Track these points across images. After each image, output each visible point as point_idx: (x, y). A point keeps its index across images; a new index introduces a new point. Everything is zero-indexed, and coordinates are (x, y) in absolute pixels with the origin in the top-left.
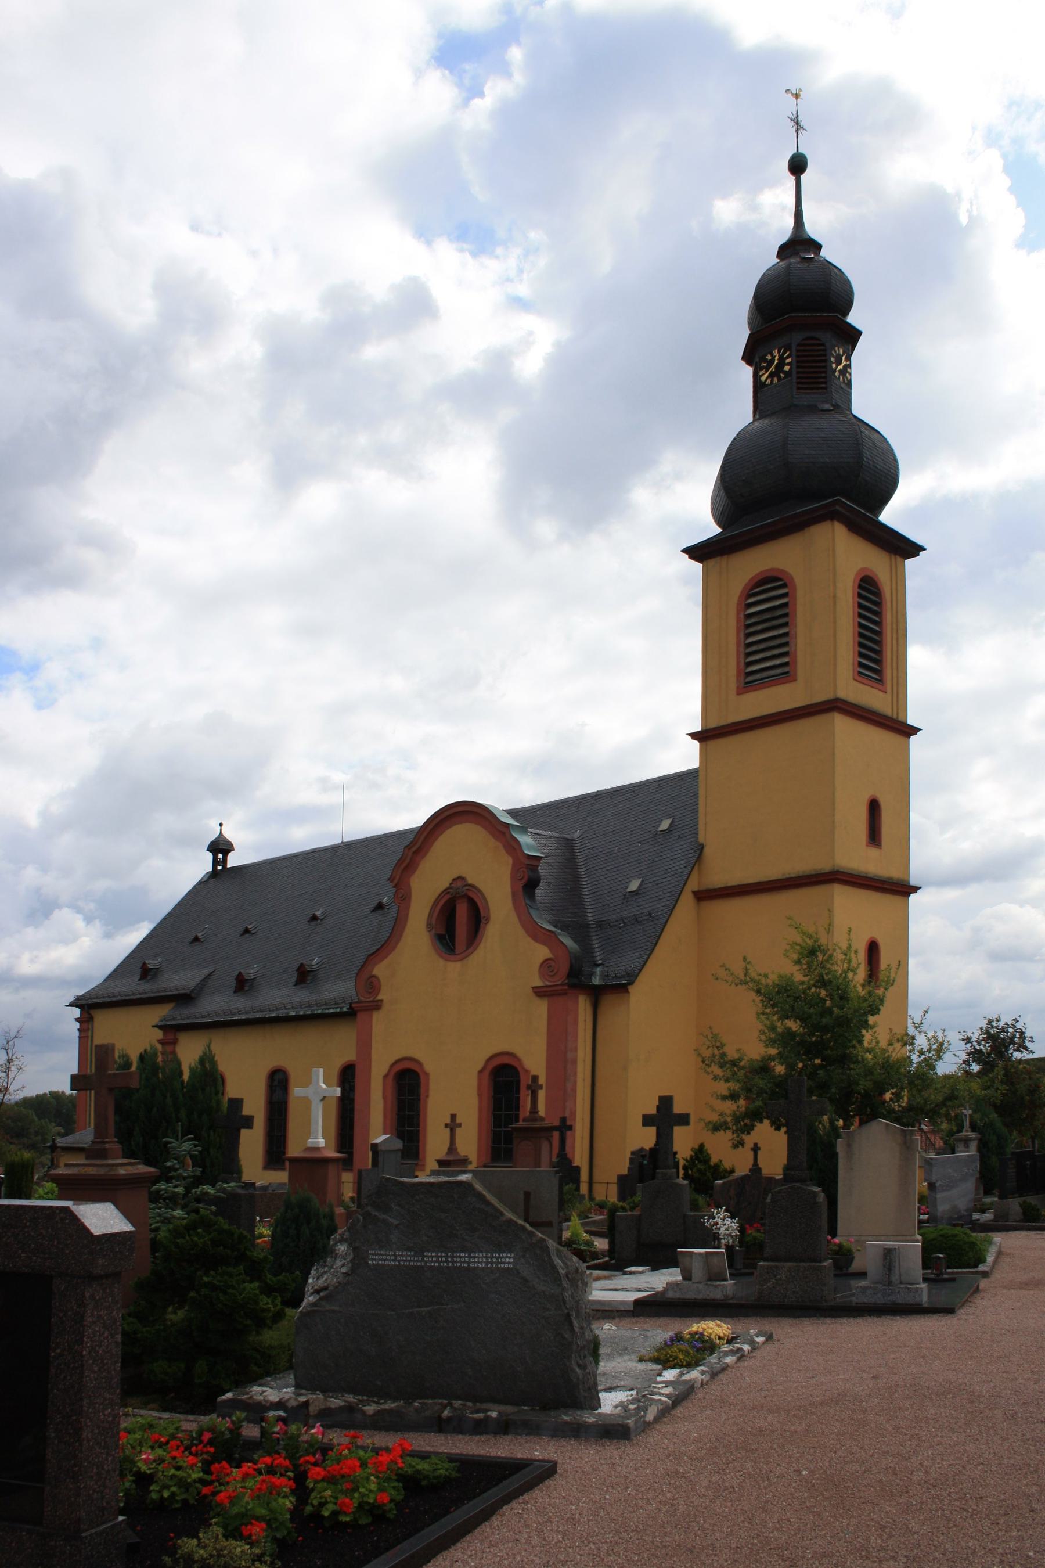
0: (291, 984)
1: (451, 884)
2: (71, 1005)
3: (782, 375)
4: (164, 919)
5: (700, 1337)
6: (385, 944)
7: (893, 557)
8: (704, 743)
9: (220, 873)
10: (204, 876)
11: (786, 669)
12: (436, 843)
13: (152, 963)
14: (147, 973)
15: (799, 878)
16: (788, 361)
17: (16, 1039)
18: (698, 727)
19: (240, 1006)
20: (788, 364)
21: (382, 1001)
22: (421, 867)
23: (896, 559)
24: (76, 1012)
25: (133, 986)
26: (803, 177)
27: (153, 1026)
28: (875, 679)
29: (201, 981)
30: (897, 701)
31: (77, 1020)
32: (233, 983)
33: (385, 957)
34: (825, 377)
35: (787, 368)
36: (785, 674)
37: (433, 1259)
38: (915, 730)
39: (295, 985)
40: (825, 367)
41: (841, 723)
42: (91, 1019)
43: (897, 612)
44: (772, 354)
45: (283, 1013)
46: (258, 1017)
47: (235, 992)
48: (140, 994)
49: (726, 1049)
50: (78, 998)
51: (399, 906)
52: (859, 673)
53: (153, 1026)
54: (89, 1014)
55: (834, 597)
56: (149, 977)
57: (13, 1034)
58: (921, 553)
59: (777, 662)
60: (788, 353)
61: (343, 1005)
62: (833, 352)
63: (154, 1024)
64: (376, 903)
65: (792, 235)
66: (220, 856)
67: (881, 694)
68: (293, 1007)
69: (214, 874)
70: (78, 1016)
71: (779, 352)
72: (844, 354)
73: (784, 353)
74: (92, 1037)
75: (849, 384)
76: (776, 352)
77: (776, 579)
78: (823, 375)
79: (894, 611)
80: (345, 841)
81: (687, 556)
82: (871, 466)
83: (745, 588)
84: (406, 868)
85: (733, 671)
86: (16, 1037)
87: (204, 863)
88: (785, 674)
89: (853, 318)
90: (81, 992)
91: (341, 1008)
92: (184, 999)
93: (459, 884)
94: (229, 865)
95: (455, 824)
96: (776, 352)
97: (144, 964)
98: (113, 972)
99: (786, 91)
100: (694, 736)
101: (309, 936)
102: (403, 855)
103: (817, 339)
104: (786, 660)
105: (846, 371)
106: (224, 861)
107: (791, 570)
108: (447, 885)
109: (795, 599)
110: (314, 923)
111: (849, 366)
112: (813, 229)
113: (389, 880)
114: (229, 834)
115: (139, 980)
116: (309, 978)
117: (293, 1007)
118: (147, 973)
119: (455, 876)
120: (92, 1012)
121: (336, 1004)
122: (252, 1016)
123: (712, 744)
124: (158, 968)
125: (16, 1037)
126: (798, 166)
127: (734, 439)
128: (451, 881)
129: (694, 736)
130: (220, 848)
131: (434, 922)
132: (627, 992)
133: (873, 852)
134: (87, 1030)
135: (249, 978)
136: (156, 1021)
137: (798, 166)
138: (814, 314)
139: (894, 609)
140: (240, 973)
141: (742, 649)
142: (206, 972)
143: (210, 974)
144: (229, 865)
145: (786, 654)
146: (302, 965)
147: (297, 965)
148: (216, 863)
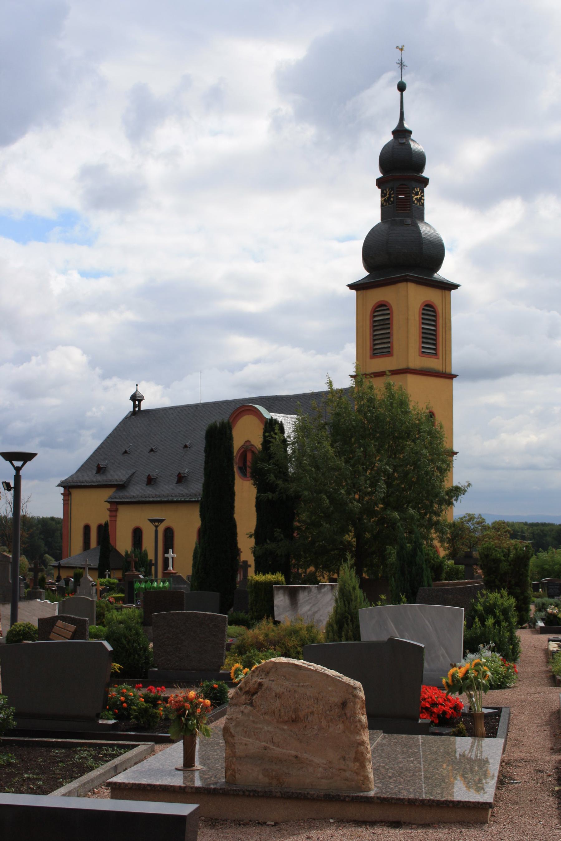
1: (244, 443)
2: (59, 485)
3: (390, 202)
4: (108, 437)
7: (444, 291)
9: (137, 412)
10: (129, 413)
11: (389, 350)
12: (238, 423)
13: (103, 464)
14: (100, 470)
16: (392, 196)
19: (150, 492)
20: (393, 197)
23: (445, 293)
24: (62, 490)
25: (91, 477)
26: (404, 93)
27: (105, 501)
28: (433, 353)
31: (62, 494)
32: (145, 479)
34: (409, 205)
35: (392, 199)
36: (388, 352)
37: (177, 586)
39: (176, 483)
40: (409, 199)
42: (70, 494)
43: (445, 318)
44: (386, 191)
45: (170, 499)
47: (147, 485)
48: (97, 482)
50: (62, 482)
52: (423, 352)
53: (105, 501)
54: (69, 491)
55: (408, 319)
56: (101, 472)
58: (459, 288)
59: (386, 346)
61: (199, 496)
62: (414, 192)
63: (105, 500)
64: (124, 451)
65: (396, 128)
66: (137, 403)
67: (436, 360)
71: (389, 190)
72: (420, 191)
73: (391, 191)
74: (71, 504)
75: (423, 205)
76: (388, 190)
77: (384, 305)
78: (409, 203)
80: (202, 402)
85: (368, 348)
86: (27, 502)
88: (388, 352)
89: (425, 174)
90: (63, 479)
91: (198, 498)
92: (121, 487)
93: (248, 444)
94: (142, 409)
95: (243, 416)
96: (388, 190)
97: (99, 465)
100: (351, 376)
103: (404, 185)
104: (389, 345)
105: (421, 201)
106: (139, 405)
107: (390, 302)
109: (392, 316)
110: (185, 449)
111: (423, 196)
114: (141, 391)
115: (96, 473)
116: (183, 480)
119: (246, 440)
120: (70, 490)
121: (195, 496)
122: (155, 499)
124: (105, 467)
125: (27, 502)
130: (136, 399)
136: (106, 498)
137: (402, 87)
140: (149, 475)
141: (372, 337)
142: (132, 472)
143: (134, 473)
144: (142, 409)
145: (389, 342)
146: (179, 473)
147: (177, 473)
148: (135, 406)
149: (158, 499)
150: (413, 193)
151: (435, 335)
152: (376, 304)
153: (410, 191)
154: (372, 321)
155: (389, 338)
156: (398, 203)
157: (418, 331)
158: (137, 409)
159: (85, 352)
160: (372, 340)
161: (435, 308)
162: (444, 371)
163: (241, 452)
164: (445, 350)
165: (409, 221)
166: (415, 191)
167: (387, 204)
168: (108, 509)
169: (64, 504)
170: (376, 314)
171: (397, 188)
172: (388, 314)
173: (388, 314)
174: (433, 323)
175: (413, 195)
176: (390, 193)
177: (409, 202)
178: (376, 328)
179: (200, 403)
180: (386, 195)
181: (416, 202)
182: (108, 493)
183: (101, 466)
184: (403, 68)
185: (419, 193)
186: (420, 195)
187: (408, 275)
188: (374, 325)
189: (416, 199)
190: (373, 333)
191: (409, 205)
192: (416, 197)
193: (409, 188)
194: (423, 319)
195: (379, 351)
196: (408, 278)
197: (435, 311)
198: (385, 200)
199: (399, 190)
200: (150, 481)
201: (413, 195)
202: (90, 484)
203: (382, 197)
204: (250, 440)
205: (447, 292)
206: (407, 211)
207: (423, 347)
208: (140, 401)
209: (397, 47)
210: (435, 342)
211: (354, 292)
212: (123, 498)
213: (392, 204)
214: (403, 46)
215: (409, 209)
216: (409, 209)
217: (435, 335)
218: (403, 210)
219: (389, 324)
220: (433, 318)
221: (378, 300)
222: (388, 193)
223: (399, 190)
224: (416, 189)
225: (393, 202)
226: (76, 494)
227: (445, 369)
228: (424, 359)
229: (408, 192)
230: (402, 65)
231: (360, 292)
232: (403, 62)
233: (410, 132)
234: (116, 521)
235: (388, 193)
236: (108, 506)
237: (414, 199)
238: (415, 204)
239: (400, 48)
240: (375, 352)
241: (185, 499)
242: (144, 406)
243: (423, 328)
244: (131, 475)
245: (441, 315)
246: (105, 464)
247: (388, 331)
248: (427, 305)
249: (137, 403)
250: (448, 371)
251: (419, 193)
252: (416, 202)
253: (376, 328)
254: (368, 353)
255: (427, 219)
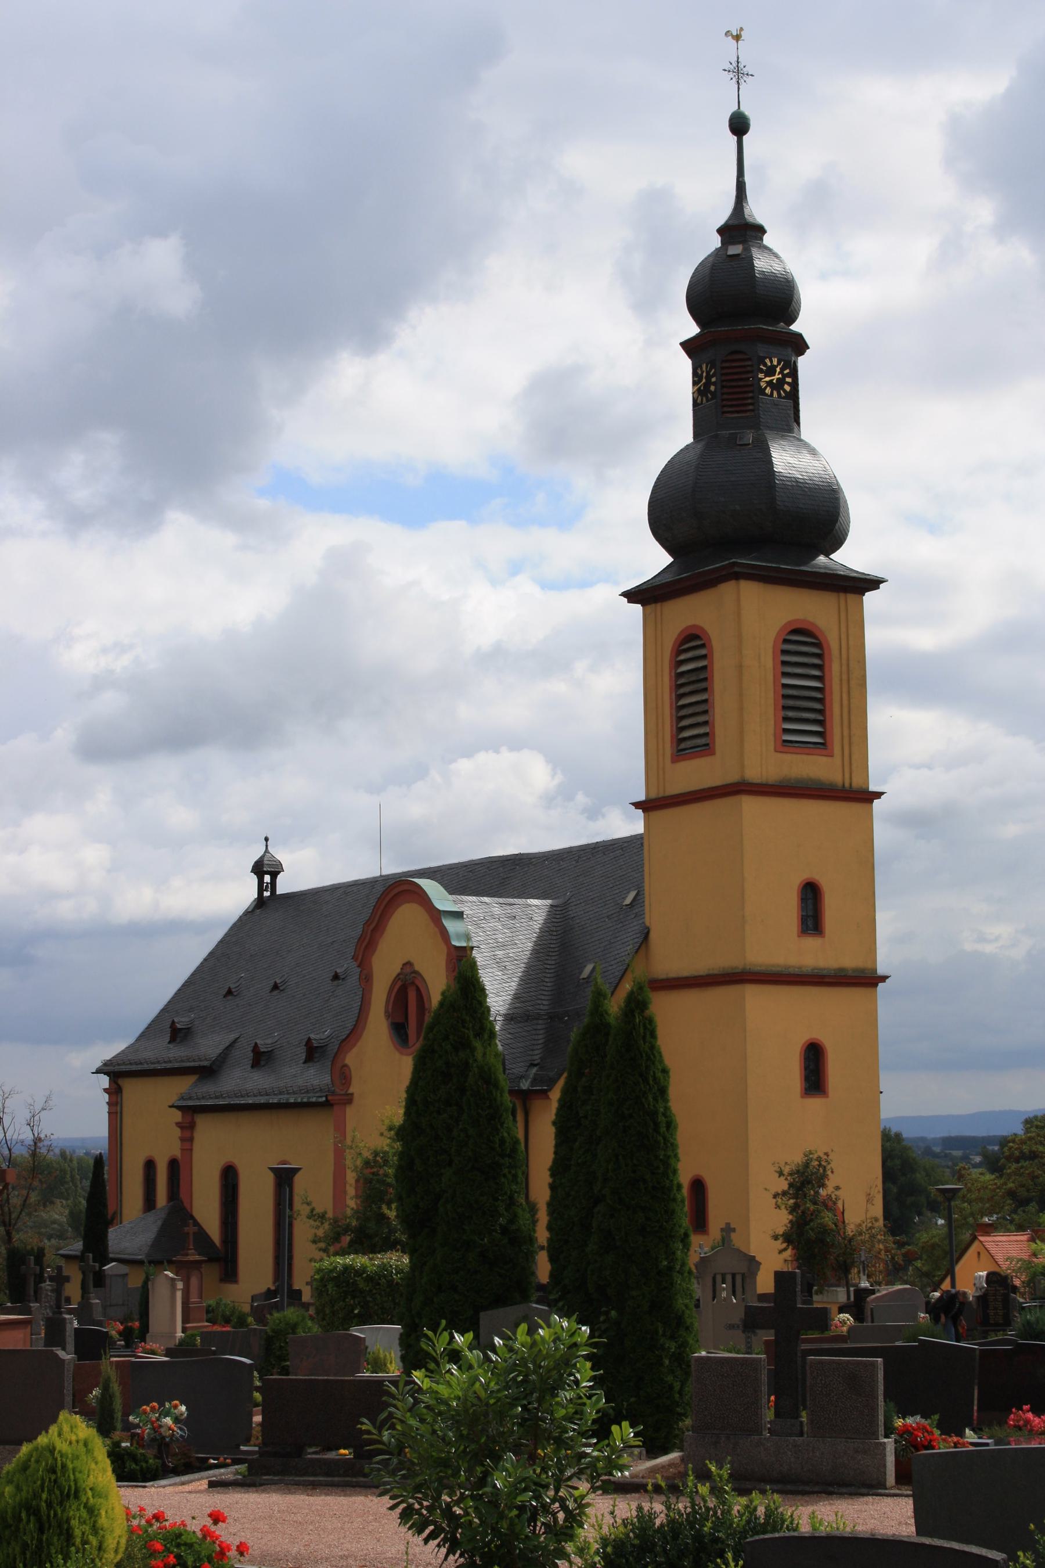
0: (302, 1061)
1: (402, 969)
2: (98, 1071)
5: (584, 1452)
6: (350, 1033)
7: (842, 595)
8: (647, 814)
13: (181, 1022)
15: (708, 976)
16: (714, 380)
17: (43, 1112)
18: (642, 797)
20: (714, 384)
21: (352, 1094)
22: (379, 947)
24: (105, 1081)
27: (170, 1107)
28: (701, 751)
29: (224, 1050)
30: (850, 764)
31: (105, 1090)
33: (354, 1045)
34: (752, 398)
35: (712, 388)
38: (878, 795)
39: (305, 1062)
41: (750, 806)
46: (250, 1102)
47: (253, 1067)
49: (314, 1205)
50: (106, 1064)
51: (363, 989)
52: (785, 741)
53: (170, 1107)
57: (38, 1108)
60: (713, 370)
63: (171, 1104)
66: (267, 878)
68: (293, 1092)
69: (260, 902)
70: (107, 1086)
76: (704, 366)
77: (696, 637)
78: (751, 395)
79: (844, 662)
80: (384, 873)
81: (626, 600)
82: (809, 493)
83: (674, 645)
84: (366, 947)
86: (43, 1109)
87: (246, 891)
92: (207, 1072)
93: (408, 970)
94: (279, 891)
96: (704, 366)
98: (146, 1028)
99: (726, 34)
100: (637, 805)
101: (329, 999)
102: (363, 931)
108: (398, 970)
109: (712, 663)
110: (336, 983)
112: (757, 211)
113: (352, 958)
115: (169, 1043)
116: (316, 1055)
117: (293, 1092)
118: (178, 1035)
119: (404, 962)
120: (120, 1081)
123: (657, 815)
124: (188, 1028)
125: (43, 1109)
126: (739, 126)
127: (666, 465)
128: (401, 966)
129: (637, 805)
131: (390, 1010)
132: (548, 1098)
133: (811, 942)
134: (117, 1104)
135: (266, 1050)
136: (173, 1099)
137: (739, 126)
138: (735, 328)
139: (844, 656)
141: (674, 711)
142: (232, 1036)
143: (235, 1041)
144: (279, 891)
145: (706, 723)
149: (262, 1100)
150: (762, 371)
151: (821, 701)
152: (679, 635)
153: (751, 366)
154: (673, 674)
155: (706, 712)
156: (725, 397)
157: (771, 695)
158: (267, 894)
159: (555, 761)
160: (674, 718)
161: (818, 634)
162: (847, 785)
163: (396, 990)
164: (850, 736)
165: (749, 437)
166: (765, 365)
167: (704, 399)
168: (178, 1124)
169: (109, 1113)
170: (682, 657)
171: (723, 361)
172: (704, 657)
173: (704, 657)
174: (816, 673)
175: (761, 376)
176: (708, 373)
177: (752, 392)
178: (682, 691)
179: (381, 876)
180: (700, 380)
181: (768, 391)
182: (178, 1087)
183: (179, 1026)
184: (741, 81)
185: (778, 370)
186: (781, 372)
187: (734, 564)
188: (679, 683)
189: (770, 383)
190: (677, 702)
191: (752, 398)
192: (768, 379)
193: (749, 359)
194: (784, 663)
195: (689, 744)
196: (736, 569)
197: (819, 645)
198: (699, 390)
199: (727, 365)
200: (260, 1058)
201: (761, 376)
202: (152, 1067)
203: (694, 383)
204: (412, 961)
205: (851, 597)
206: (748, 414)
207: (786, 731)
208: (274, 875)
209: (728, 33)
210: (821, 718)
211: (638, 608)
212: (203, 1098)
213: (712, 399)
214: (741, 29)
215: (751, 407)
216: (751, 407)
217: (821, 701)
218: (738, 412)
219: (705, 679)
220: (816, 661)
221: (684, 625)
222: (704, 374)
223: (727, 365)
224: (767, 361)
225: (713, 394)
226: (131, 1088)
227: (851, 778)
228: (788, 757)
229: (749, 369)
230: (738, 73)
231: (649, 608)
232: (741, 66)
233: (760, 230)
234: (191, 1150)
235: (704, 374)
236: (178, 1116)
237: (763, 385)
238: (766, 395)
239: (735, 33)
240: (683, 746)
241: (309, 1098)
242: (285, 885)
243: (784, 686)
244: (230, 1046)
245: (835, 652)
246: (186, 1019)
247: (704, 697)
248: (796, 631)
249: (267, 878)
250: (857, 783)
251: (778, 370)
252: (768, 391)
253: (682, 691)
254: (668, 749)
255: (809, 426)
